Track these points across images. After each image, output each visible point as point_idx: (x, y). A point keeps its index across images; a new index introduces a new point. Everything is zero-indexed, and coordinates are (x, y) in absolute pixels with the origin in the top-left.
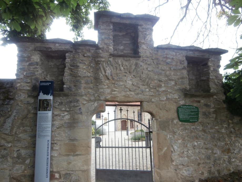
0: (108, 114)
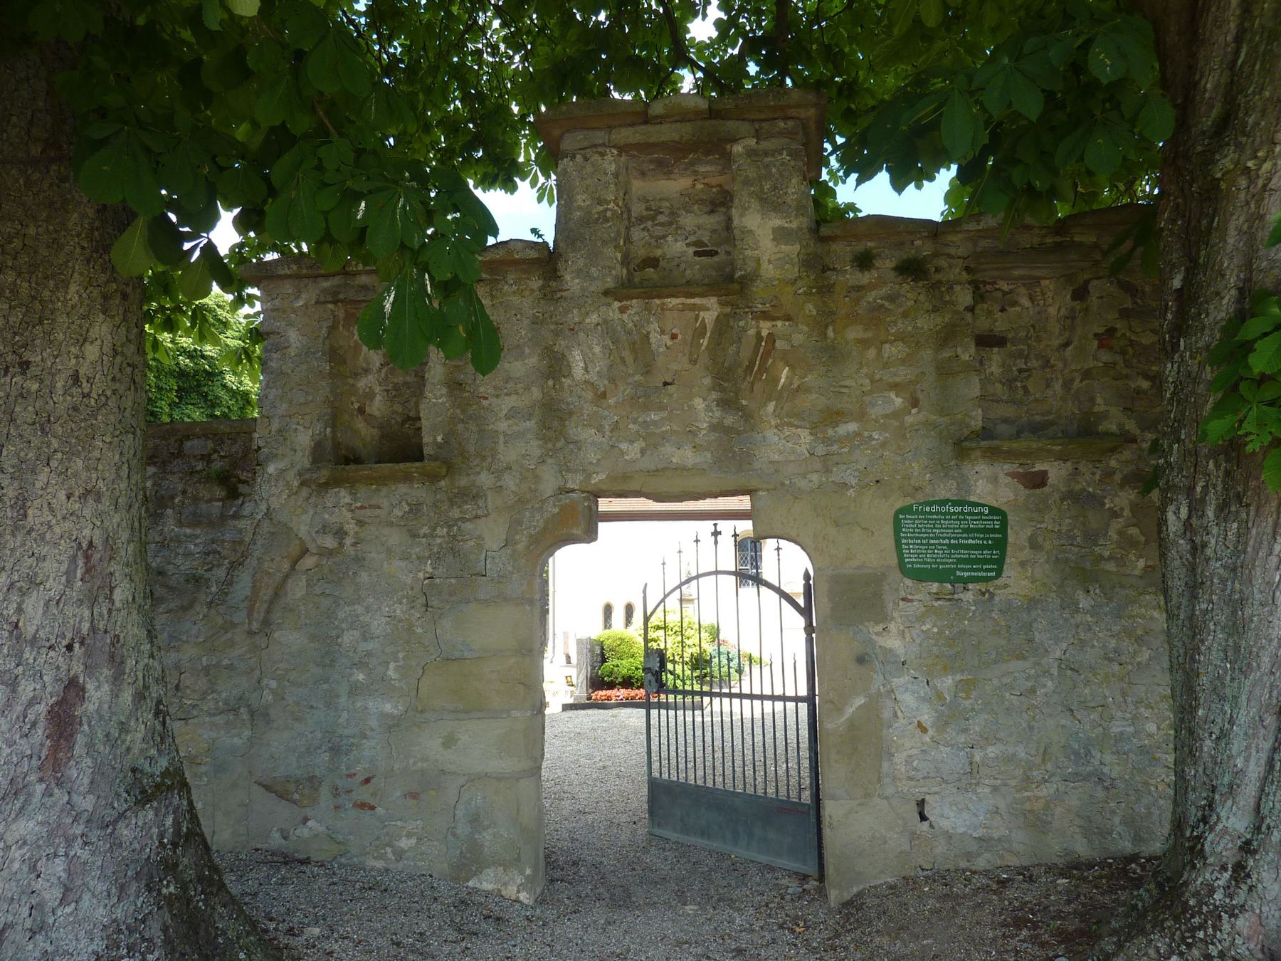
0: (697, 541)
